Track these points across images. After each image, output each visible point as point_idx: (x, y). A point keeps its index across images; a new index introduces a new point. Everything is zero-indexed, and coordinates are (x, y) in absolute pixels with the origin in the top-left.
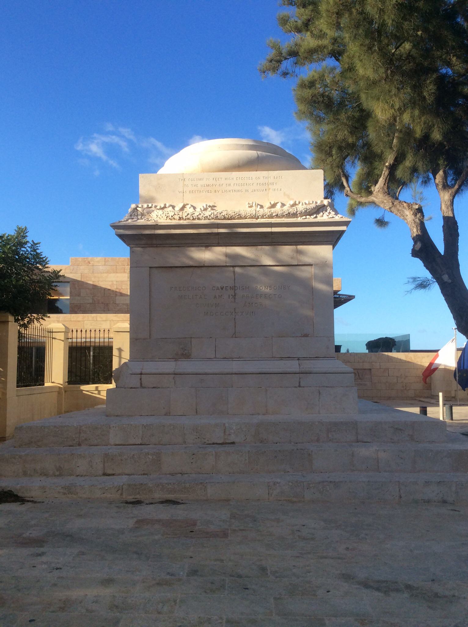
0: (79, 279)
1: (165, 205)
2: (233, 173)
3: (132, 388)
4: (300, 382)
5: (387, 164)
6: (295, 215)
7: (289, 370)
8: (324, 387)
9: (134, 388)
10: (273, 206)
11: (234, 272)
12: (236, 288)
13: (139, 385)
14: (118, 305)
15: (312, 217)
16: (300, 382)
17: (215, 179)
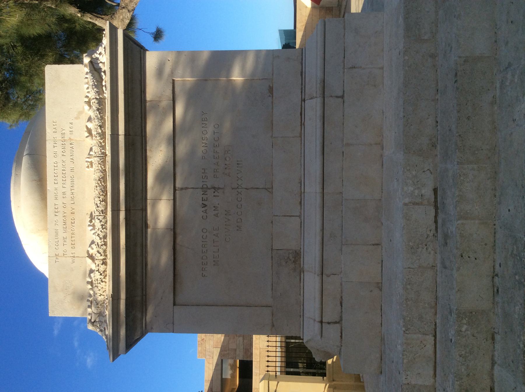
0: (219, 350)
1: (88, 283)
2: (48, 188)
3: (341, 337)
4: (337, 97)
5: (79, 15)
6: (101, 102)
7: (319, 113)
8: (344, 62)
9: (342, 333)
10: (89, 131)
11: (182, 189)
12: (205, 186)
15: (104, 77)
16: (337, 97)
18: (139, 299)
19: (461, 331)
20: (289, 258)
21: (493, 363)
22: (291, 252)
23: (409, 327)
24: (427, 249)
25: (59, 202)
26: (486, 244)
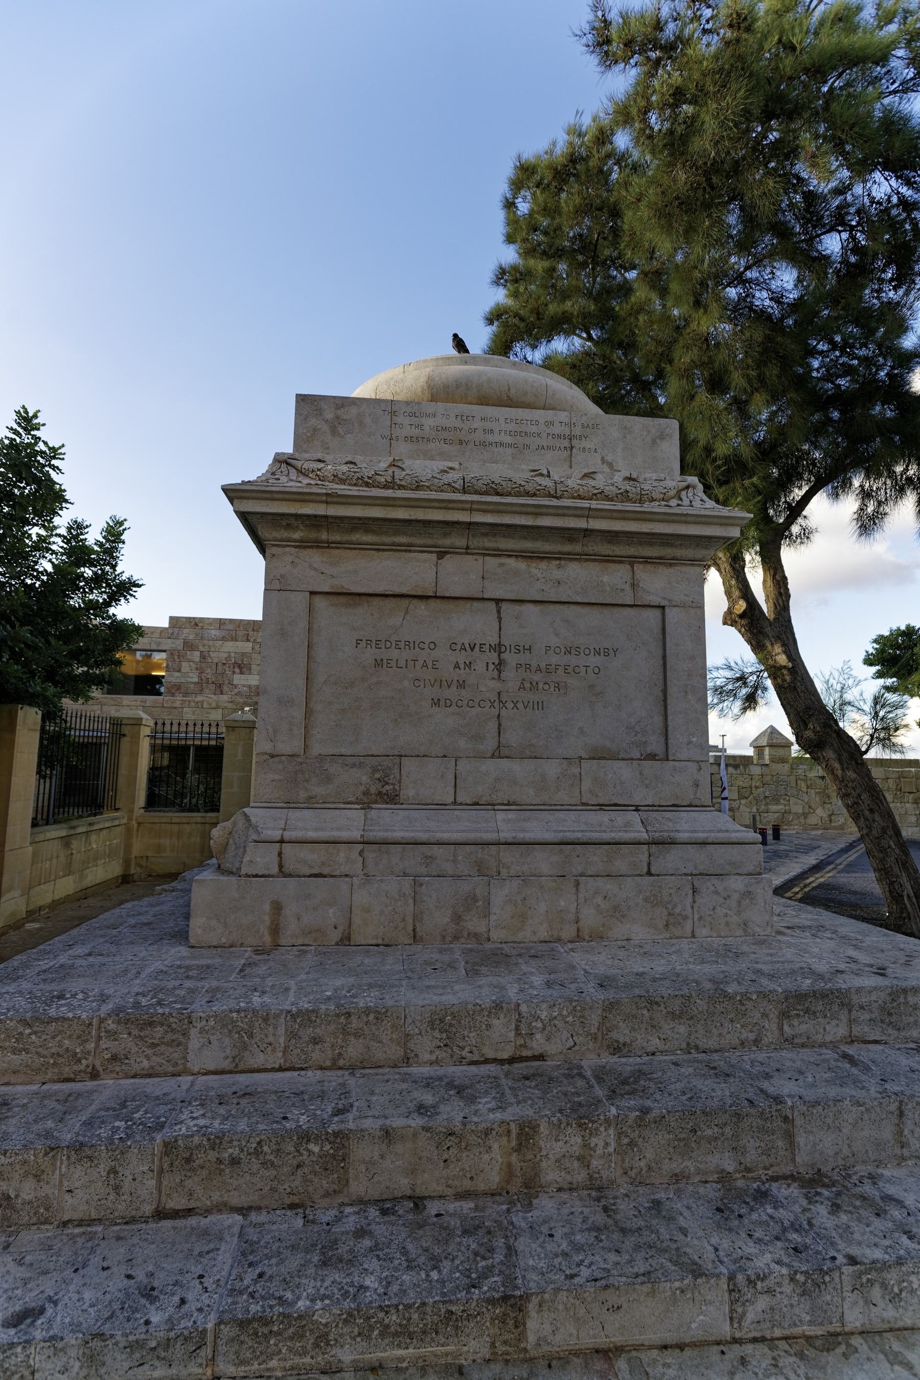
4: (649, 865)
12: (503, 649)
13: (275, 870)
14: (236, 686)
17: (460, 417)
18: (324, 536)
19: (309, 1141)
20: (387, 783)
21: (243, 1211)
22: (397, 787)
23: (298, 1020)
24: (439, 1047)
25: (476, 424)
26: (472, 1178)
